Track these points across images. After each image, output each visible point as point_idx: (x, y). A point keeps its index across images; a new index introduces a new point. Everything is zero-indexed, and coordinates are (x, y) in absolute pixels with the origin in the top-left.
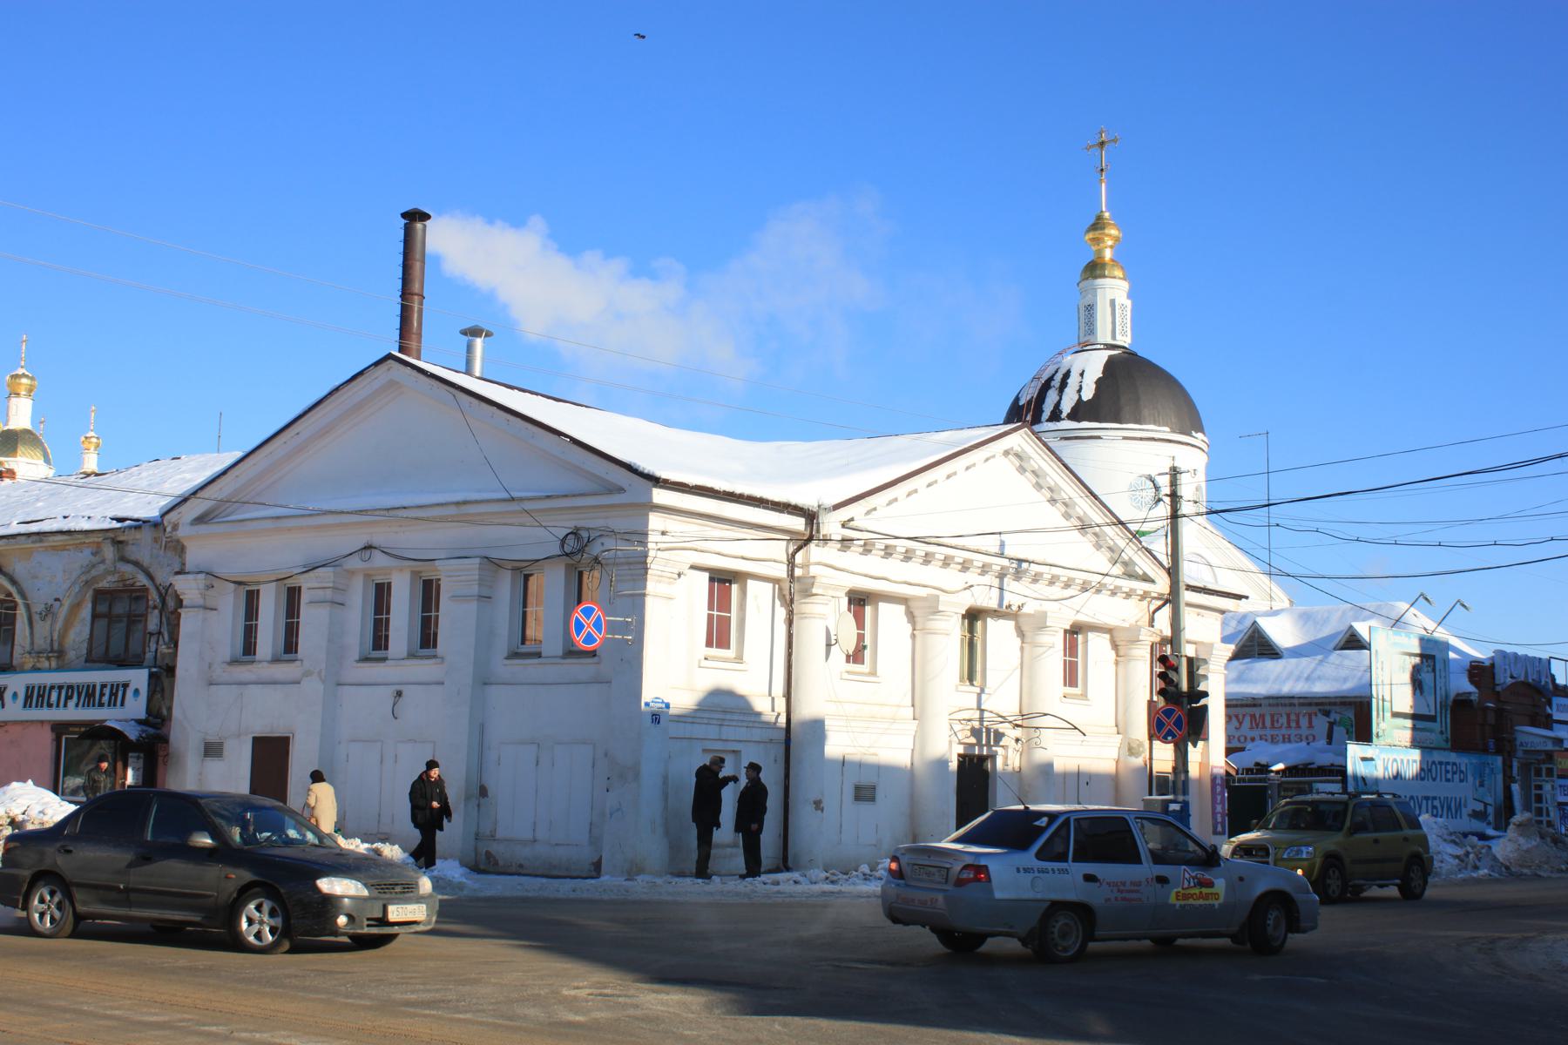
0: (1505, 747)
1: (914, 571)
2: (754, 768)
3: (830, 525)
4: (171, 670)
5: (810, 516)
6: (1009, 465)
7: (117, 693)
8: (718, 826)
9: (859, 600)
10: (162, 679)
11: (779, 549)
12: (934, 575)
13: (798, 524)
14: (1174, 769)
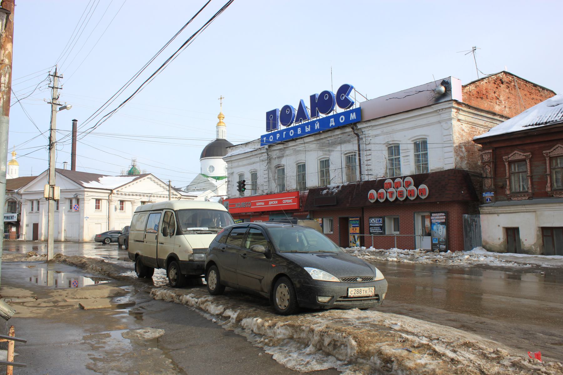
0: (220, 120)
1: (131, 197)
2: (241, 176)
3: (115, 191)
4: (20, 214)
5: (111, 190)
6: (149, 180)
7: (12, 217)
8: (288, 300)
9: (122, 202)
10: (19, 214)
11: (107, 195)
12: (135, 197)
13: (110, 192)
14: (288, 192)
